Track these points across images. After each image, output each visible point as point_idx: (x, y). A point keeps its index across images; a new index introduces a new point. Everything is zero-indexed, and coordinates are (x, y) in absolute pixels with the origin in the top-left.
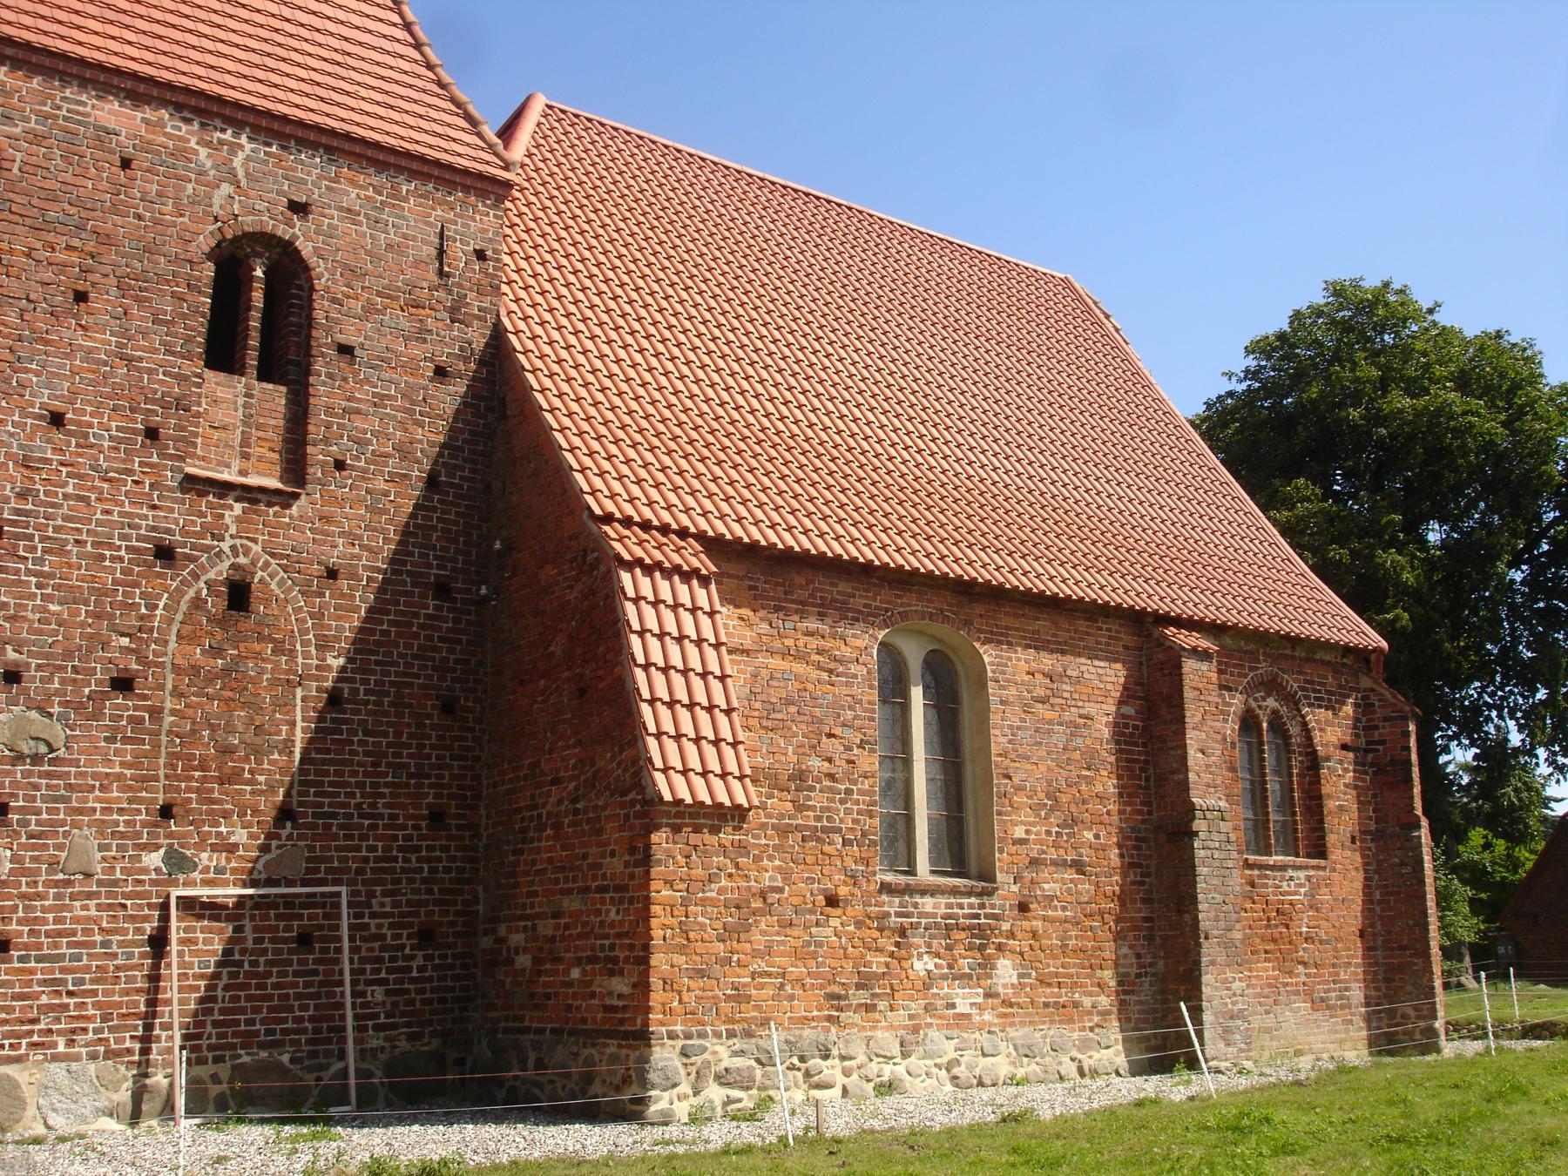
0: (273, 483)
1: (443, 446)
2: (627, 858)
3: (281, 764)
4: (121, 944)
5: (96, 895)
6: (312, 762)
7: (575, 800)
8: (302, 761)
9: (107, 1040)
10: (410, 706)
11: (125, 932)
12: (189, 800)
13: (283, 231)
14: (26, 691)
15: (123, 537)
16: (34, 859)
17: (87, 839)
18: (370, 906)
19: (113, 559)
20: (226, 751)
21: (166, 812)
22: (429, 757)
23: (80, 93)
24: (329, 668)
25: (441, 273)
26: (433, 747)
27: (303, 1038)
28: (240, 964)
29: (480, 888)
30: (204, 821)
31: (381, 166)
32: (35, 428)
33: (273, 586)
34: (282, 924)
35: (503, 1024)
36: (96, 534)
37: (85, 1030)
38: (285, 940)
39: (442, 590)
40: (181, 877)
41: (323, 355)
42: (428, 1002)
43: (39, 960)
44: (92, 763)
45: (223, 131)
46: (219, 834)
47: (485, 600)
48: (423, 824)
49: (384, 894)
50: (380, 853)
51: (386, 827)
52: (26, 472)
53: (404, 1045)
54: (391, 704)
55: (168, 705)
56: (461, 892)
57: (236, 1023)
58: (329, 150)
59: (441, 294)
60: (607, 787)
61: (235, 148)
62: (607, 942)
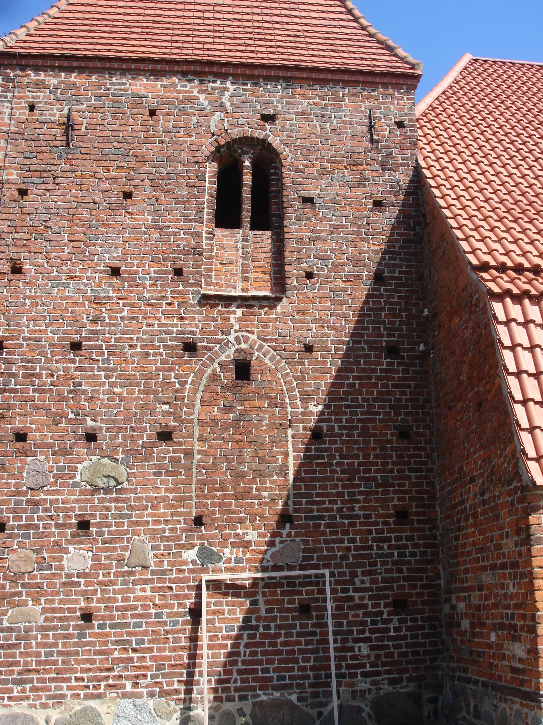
0: (268, 294)
1: (384, 253)
2: (516, 538)
3: (279, 483)
4: (169, 615)
5: (151, 581)
6: (303, 480)
7: (482, 494)
8: (295, 480)
9: (161, 683)
10: (375, 435)
11: (171, 606)
12: (214, 512)
13: (258, 134)
14: (100, 446)
15: (161, 340)
16: (108, 558)
17: (143, 542)
18: (353, 583)
19: (155, 355)
20: (239, 476)
21: (198, 521)
22: (392, 471)
23: (122, 78)
24: (311, 413)
25: (372, 141)
26: (394, 463)
27: (307, 682)
28: (257, 628)
29: (440, 567)
30: (225, 527)
31: (323, 83)
32: (101, 279)
33: (267, 361)
34: (286, 598)
35: (457, 674)
36: (143, 340)
37: (145, 676)
38: (289, 610)
39: (392, 351)
40: (211, 566)
41: (292, 206)
42: (405, 654)
43: (112, 627)
44: (145, 490)
45: (214, 82)
46: (236, 535)
47: (424, 355)
48: (391, 520)
49: (364, 574)
50: (358, 544)
51: (361, 524)
52: (95, 306)
53: (386, 688)
54: (359, 435)
55: (197, 447)
56: (425, 570)
57: (255, 671)
58: (286, 79)
59: (374, 154)
60: (499, 480)
61: (222, 91)
62: (509, 612)
